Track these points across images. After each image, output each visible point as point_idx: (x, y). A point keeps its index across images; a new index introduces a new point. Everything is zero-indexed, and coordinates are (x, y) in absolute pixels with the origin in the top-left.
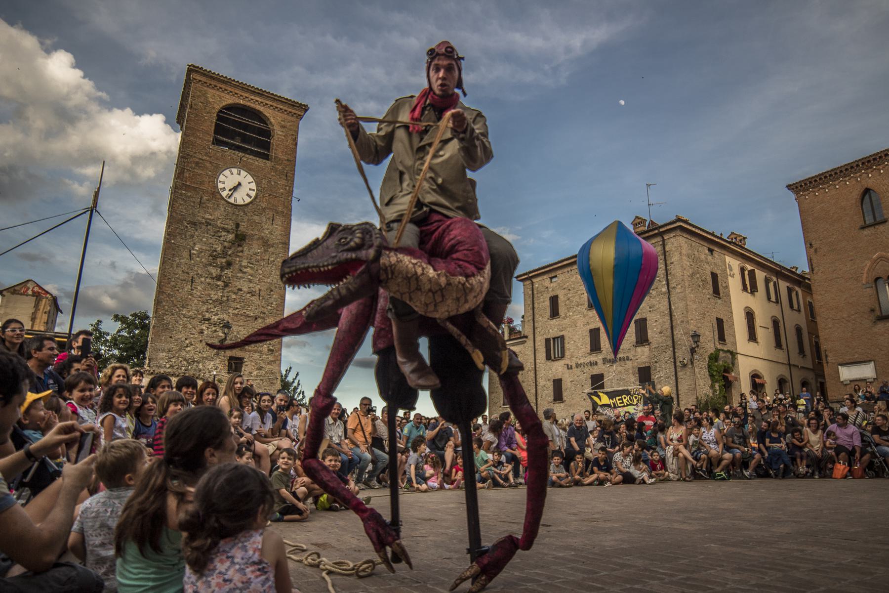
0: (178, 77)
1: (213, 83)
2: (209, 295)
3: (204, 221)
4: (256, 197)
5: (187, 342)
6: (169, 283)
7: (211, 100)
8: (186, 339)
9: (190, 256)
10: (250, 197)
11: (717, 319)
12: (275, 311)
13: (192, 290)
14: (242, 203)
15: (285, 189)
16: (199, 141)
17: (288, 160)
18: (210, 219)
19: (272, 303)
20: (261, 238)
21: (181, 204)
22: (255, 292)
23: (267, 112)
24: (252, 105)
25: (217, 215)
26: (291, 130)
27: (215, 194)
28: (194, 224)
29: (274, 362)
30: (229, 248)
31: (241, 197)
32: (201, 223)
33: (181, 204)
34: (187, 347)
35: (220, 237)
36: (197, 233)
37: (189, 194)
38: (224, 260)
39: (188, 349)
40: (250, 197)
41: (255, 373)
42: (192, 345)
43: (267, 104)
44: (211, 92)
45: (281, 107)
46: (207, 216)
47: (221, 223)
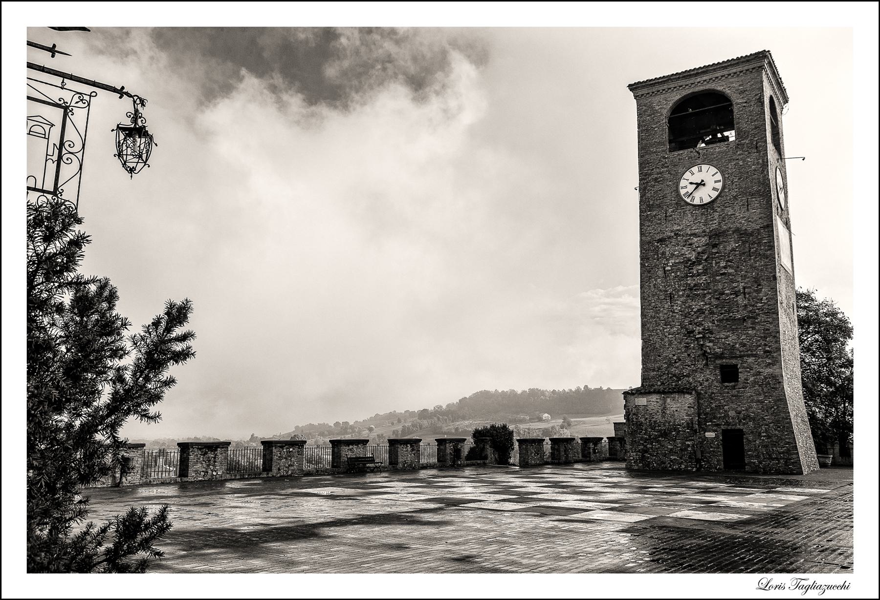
0: (175, 455)
1: (655, 89)
2: (690, 307)
3: (673, 234)
4: (724, 187)
5: (675, 358)
6: (650, 305)
7: (657, 108)
8: (674, 355)
9: (665, 273)
10: (719, 181)
11: (123, 87)
12: (766, 306)
13: (672, 306)
14: (709, 200)
15: (758, 163)
16: (654, 156)
17: (756, 128)
18: (677, 230)
19: (762, 299)
20: (737, 230)
21: (649, 226)
22: (740, 291)
23: (719, 87)
24: (701, 88)
25: (687, 223)
26: (753, 90)
27: (680, 203)
28: (661, 241)
29: (773, 364)
30: (703, 253)
31: (705, 195)
32: (670, 237)
33: (649, 226)
34: (676, 362)
35: (691, 244)
36: (667, 249)
37: (654, 213)
38: (700, 267)
39: (677, 364)
40: (719, 181)
41: (752, 379)
42: (680, 360)
43: (717, 78)
44: (655, 100)
45: (734, 71)
46: (676, 227)
47: (690, 230)
